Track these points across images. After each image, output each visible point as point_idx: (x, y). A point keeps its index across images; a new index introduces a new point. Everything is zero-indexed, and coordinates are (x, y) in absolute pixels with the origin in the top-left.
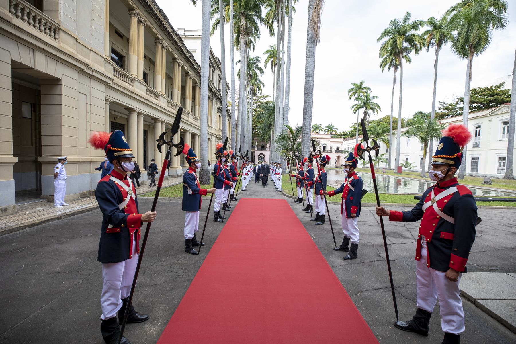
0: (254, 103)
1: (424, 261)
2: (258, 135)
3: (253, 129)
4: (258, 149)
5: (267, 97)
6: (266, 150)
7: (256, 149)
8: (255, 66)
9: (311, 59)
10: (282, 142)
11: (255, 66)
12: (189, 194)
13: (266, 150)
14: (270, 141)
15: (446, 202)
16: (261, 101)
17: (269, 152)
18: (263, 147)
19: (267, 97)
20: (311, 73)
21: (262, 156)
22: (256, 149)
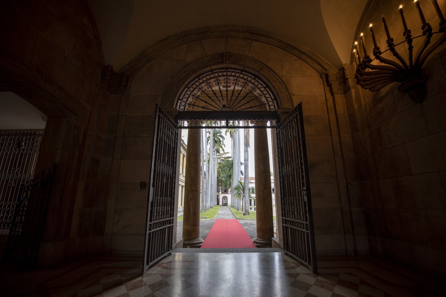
0: (219, 158)
1: (170, 252)
2: (222, 181)
3: (218, 178)
4: (222, 193)
5: (227, 153)
6: (228, 193)
7: (220, 193)
8: (219, 134)
11: (219, 134)
13: (228, 193)
14: (230, 186)
16: (223, 156)
17: (230, 195)
18: (225, 191)
19: (227, 153)
20: (247, 159)
21: (225, 198)
22: (220, 193)
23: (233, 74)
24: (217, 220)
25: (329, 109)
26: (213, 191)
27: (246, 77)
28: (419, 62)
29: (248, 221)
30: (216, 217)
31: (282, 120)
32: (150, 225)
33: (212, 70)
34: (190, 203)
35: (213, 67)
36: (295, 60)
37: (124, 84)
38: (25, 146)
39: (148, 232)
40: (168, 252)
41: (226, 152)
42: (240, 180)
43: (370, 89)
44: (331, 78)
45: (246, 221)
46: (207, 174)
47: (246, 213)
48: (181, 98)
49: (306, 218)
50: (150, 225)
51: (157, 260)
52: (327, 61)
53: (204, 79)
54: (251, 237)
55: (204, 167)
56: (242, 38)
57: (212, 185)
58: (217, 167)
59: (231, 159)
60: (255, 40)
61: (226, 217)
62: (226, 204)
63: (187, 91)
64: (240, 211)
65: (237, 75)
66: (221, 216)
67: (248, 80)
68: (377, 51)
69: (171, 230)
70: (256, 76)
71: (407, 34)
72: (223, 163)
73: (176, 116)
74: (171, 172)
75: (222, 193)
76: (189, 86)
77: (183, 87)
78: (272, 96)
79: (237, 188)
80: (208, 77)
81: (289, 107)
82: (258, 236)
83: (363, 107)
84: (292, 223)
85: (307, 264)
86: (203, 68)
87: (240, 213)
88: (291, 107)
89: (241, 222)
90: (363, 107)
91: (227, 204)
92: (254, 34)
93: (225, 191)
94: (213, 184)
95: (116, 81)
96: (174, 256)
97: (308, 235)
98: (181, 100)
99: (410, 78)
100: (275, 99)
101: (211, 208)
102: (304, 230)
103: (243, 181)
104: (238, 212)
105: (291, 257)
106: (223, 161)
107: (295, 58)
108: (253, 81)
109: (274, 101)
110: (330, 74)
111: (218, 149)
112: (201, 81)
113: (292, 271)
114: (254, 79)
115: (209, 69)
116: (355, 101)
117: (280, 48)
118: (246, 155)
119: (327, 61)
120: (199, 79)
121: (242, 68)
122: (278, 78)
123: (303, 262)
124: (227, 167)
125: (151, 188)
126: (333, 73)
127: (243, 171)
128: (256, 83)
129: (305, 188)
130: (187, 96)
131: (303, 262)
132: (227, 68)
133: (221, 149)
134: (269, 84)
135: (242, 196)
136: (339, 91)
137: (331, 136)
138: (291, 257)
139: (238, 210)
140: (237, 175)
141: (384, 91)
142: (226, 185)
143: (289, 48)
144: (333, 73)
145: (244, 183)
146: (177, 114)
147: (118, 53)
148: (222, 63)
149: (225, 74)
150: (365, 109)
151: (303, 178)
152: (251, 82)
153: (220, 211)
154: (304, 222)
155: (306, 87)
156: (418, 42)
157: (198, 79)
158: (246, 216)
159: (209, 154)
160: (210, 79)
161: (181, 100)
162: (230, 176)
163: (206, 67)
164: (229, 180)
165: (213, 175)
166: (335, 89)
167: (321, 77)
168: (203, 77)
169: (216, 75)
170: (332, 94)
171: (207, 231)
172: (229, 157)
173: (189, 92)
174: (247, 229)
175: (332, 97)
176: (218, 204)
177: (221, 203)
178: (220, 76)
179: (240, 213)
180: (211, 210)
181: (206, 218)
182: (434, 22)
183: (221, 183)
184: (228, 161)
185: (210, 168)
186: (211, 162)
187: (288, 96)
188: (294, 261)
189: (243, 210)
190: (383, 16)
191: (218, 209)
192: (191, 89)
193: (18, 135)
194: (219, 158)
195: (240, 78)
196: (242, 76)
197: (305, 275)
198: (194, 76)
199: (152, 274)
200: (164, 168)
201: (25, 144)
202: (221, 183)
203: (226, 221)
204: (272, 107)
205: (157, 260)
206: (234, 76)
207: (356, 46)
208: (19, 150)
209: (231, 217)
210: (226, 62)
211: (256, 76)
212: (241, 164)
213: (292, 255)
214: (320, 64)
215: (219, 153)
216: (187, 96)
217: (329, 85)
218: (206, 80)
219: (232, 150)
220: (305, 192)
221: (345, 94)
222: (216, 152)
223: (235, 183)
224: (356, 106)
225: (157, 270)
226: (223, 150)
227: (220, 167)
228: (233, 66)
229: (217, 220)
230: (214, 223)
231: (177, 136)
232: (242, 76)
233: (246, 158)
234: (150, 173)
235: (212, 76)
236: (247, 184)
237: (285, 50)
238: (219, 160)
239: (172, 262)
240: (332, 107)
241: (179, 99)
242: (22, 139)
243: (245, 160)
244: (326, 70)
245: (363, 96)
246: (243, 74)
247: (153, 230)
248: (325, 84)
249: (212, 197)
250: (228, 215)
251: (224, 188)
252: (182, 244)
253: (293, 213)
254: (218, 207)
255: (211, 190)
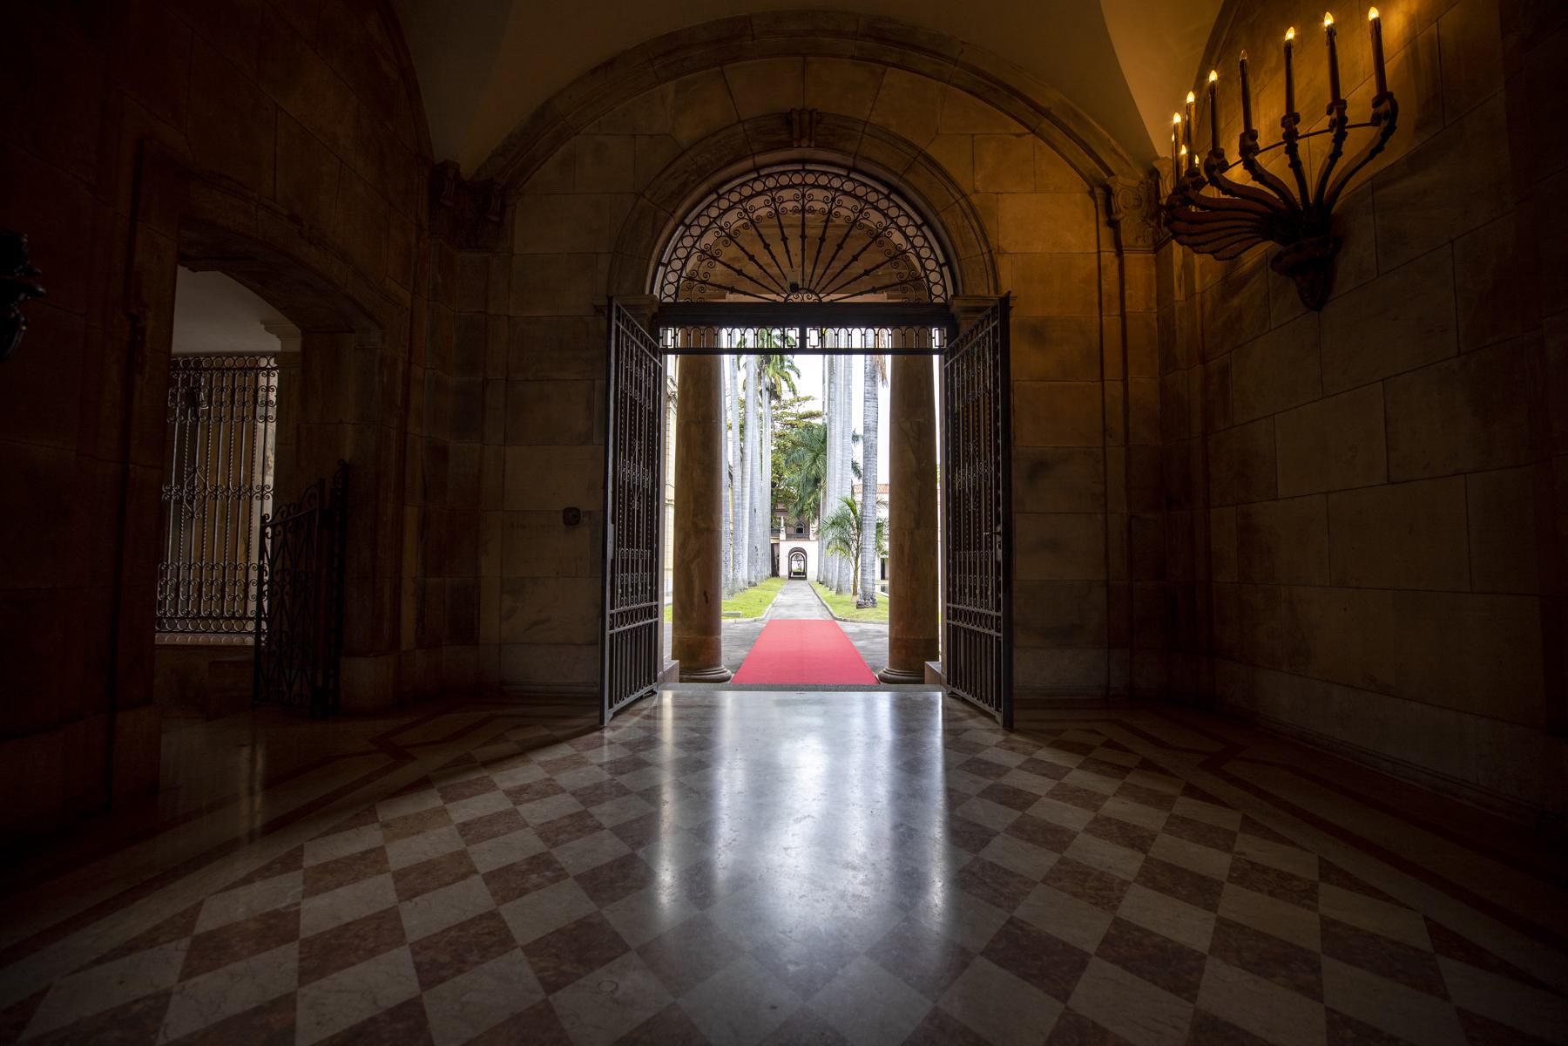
0: (776, 418)
1: (653, 686)
2: (787, 498)
3: (773, 485)
4: (789, 537)
5: (807, 399)
7: (783, 536)
9: (872, 403)
10: (835, 531)
12: (724, 332)
14: (817, 515)
15: (1197, 100)
16: (793, 410)
18: (800, 531)
19: (807, 399)
20: (872, 425)
21: (798, 553)
22: (783, 536)
23: (823, 180)
24: (772, 623)
25: (1104, 298)
26: (758, 530)
27: (861, 191)
28: (1324, 201)
29: (870, 627)
30: (768, 613)
31: (964, 330)
32: (612, 616)
33: (757, 169)
34: (693, 566)
35: (761, 159)
36: (1018, 135)
37: (495, 219)
38: (210, 404)
39: (608, 632)
40: (646, 689)
41: (801, 394)
42: (848, 494)
43: (1212, 253)
44: (1118, 202)
45: (864, 626)
46: (737, 473)
47: (866, 601)
48: (665, 260)
49: (998, 601)
50: (612, 616)
51: (627, 701)
52: (1113, 142)
53: (735, 197)
54: (875, 668)
55: (729, 453)
56: (852, 57)
57: (753, 511)
58: (769, 447)
59: (818, 421)
60: (894, 65)
61: (801, 614)
62: (800, 575)
63: (682, 238)
64: (848, 597)
65: (836, 183)
66: (784, 613)
67: (867, 202)
68: (1215, 161)
69: (653, 631)
70: (893, 189)
71: (1290, 119)
72: (793, 434)
73: (654, 316)
74: (648, 479)
75: (789, 537)
76: (687, 221)
77: (672, 223)
78: (938, 252)
79: (838, 522)
80: (747, 191)
81: (985, 293)
82: (893, 663)
83: (1198, 298)
84: (969, 617)
85: (992, 710)
86: (729, 164)
87: (846, 603)
88: (992, 293)
89: (848, 628)
90: (1198, 298)
91: (804, 573)
92: (891, 44)
93: (800, 531)
94: (757, 505)
95: (471, 209)
96: (661, 697)
97: (998, 642)
98: (666, 266)
99: (1301, 234)
100: (948, 263)
101: (752, 584)
102: (993, 632)
103: (859, 498)
104: (839, 598)
105: (963, 700)
106: (793, 426)
107: (1017, 127)
108: (883, 204)
109: (945, 269)
110: (1116, 188)
111: (774, 386)
112: (724, 204)
113: (957, 725)
114: (887, 197)
115: (748, 164)
116: (1180, 280)
117: (971, 93)
118: (871, 412)
119: (1113, 142)
120: (720, 197)
121: (850, 162)
122: (958, 196)
123: (986, 707)
124: (805, 448)
125: (610, 526)
126: (1127, 183)
127: (861, 465)
128: (893, 212)
129: (999, 528)
130: (682, 253)
131: (986, 707)
132: (803, 161)
133: (784, 384)
134: (931, 216)
135: (854, 545)
136: (1140, 243)
137: (1102, 380)
138: (963, 700)
139: (839, 592)
140: (838, 476)
141: (1251, 258)
142: (802, 511)
143: (1000, 92)
144: (1127, 183)
145: (864, 506)
146: (656, 310)
147: (470, 123)
148: (788, 145)
149: (797, 179)
150: (1202, 306)
151: (998, 504)
152: (876, 208)
153: (780, 596)
154: (993, 613)
155: (1044, 230)
156: (1314, 150)
157: (714, 196)
158: (865, 611)
159: (743, 403)
160: (751, 196)
161: (666, 266)
162: (816, 481)
163: (738, 159)
164: (812, 492)
165: (757, 475)
166: (1127, 237)
167: (1091, 193)
168: (731, 191)
169: (771, 183)
170: (1119, 253)
171: (743, 653)
172: (812, 415)
173: (688, 242)
174: (863, 648)
175: (1116, 262)
176: (775, 573)
177: (783, 571)
178: (782, 188)
179: (846, 603)
180: (752, 591)
181: (738, 615)
182: (1360, 96)
183: (786, 503)
184: (809, 428)
185: (748, 451)
186: (753, 431)
187: (987, 257)
188: (967, 708)
189: (855, 593)
190: (1243, 55)
191: (776, 590)
192: (696, 231)
193: (184, 370)
194: (776, 418)
195: (845, 193)
196: (848, 186)
197: (987, 734)
198: (703, 188)
199: (619, 729)
200: (634, 473)
201: (210, 396)
202: (786, 503)
203: (802, 625)
204: (937, 290)
205: (627, 701)
206: (825, 187)
207: (1176, 127)
208: (195, 413)
209: (816, 614)
210: (798, 134)
211: (893, 189)
212: (855, 438)
213: (964, 694)
214: (1091, 152)
215: (778, 398)
216: (682, 253)
217: (1113, 224)
218: (741, 201)
219: (811, 421)
220: (999, 539)
221: (1156, 251)
222: (766, 395)
223: (833, 505)
224: (1179, 295)
225: (629, 723)
226: (793, 390)
227: (781, 449)
228: (822, 155)
229: (771, 621)
230: (761, 632)
231: (659, 374)
232: (848, 186)
233: (870, 421)
234: (614, 492)
235: (759, 186)
236: (869, 510)
237: (986, 101)
238: (777, 425)
239: (659, 707)
240: (1116, 290)
241: (659, 263)
242: (197, 381)
243: (866, 429)
244: (1110, 173)
245: (1202, 266)
246: (852, 180)
247: (617, 630)
248: (1102, 219)
249: (753, 550)
250: (808, 607)
251: (794, 521)
252: (676, 674)
253: (972, 593)
254: (774, 583)
255: (751, 527)
